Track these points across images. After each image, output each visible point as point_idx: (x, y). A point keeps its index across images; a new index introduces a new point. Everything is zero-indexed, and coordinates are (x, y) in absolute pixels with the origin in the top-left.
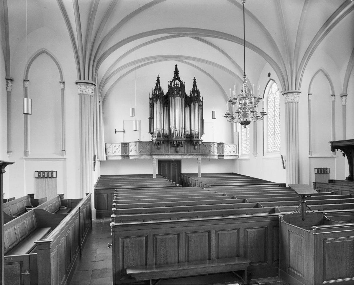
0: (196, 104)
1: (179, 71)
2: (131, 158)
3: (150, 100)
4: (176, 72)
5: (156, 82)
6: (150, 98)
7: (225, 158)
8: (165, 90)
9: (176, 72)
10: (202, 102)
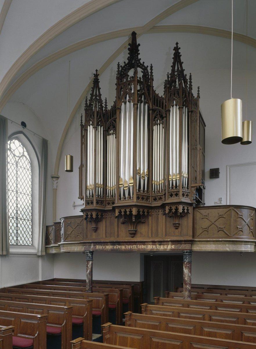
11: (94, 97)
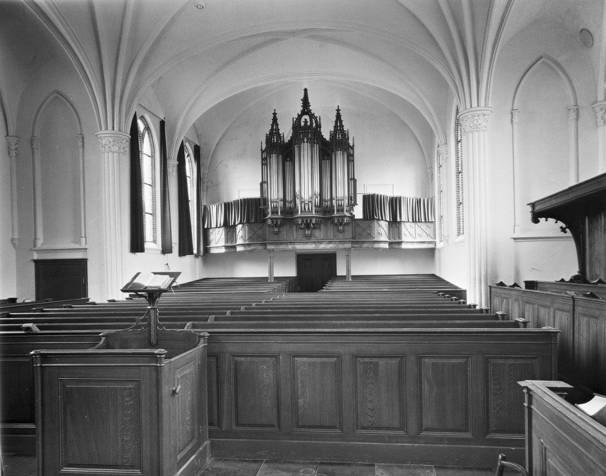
0: (339, 153)
1: (302, 100)
2: (239, 249)
3: (262, 152)
4: (306, 102)
5: (335, 119)
6: (261, 150)
7: (404, 246)
8: (286, 132)
9: (306, 102)
10: (352, 148)
11: (274, 131)
